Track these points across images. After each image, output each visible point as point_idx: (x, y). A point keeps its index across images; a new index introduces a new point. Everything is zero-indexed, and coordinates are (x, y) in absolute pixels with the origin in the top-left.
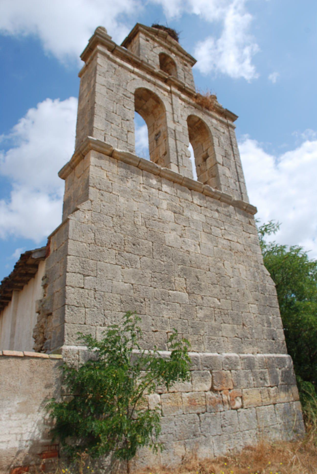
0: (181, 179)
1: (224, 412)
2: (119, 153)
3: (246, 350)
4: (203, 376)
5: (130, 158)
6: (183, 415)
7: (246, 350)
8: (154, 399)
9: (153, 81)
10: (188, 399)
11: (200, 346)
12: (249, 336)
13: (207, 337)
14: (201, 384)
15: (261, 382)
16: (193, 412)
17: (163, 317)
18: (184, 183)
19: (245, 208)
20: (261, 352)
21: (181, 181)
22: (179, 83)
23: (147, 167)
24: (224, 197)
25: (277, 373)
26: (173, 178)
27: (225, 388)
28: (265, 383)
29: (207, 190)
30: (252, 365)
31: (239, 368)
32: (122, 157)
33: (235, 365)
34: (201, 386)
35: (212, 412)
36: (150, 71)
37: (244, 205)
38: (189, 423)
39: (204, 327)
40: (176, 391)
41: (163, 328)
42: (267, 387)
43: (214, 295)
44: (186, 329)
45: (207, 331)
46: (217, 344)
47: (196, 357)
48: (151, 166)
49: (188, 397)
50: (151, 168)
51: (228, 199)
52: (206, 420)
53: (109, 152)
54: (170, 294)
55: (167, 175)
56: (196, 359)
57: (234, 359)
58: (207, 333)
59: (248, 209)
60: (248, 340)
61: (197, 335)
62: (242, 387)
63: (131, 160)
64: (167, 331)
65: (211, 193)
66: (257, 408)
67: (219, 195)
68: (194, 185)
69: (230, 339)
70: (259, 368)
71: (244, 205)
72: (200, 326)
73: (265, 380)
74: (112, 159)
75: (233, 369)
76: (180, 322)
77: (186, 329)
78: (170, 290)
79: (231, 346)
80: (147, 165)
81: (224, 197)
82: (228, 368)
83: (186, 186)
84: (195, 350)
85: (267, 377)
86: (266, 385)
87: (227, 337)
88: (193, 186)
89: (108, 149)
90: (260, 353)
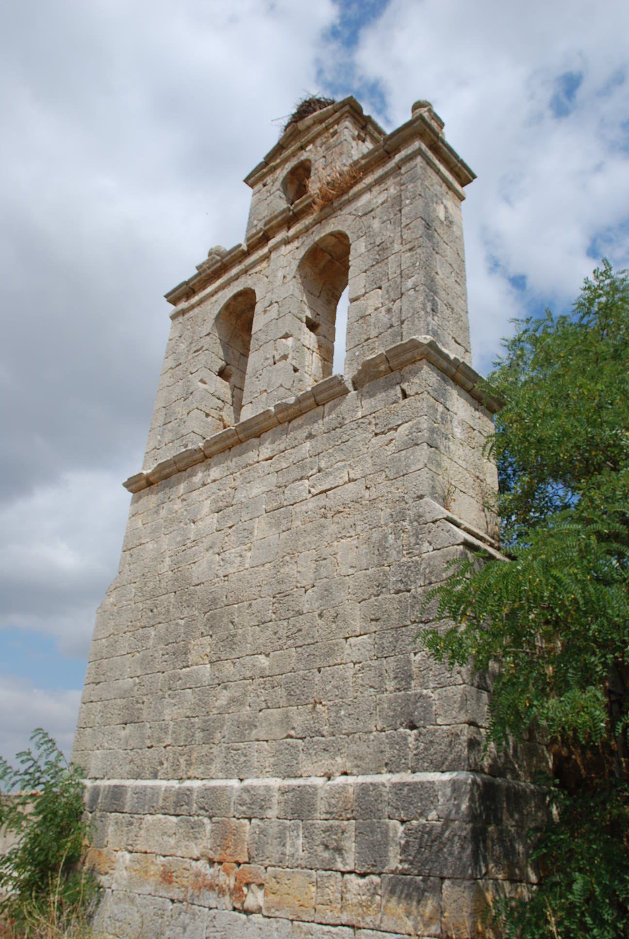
0: (233, 435)
1: (216, 911)
2: (153, 473)
3: (306, 766)
4: (193, 828)
5: (164, 469)
6: (149, 897)
7: (306, 766)
8: (121, 860)
9: (310, 224)
10: (162, 868)
11: (209, 766)
12: (326, 729)
13: (226, 745)
14: (187, 843)
15: (326, 855)
16: (165, 895)
17: (164, 720)
18: (241, 436)
19: (382, 368)
20: (355, 771)
21: (237, 437)
22: (280, 218)
23: (186, 461)
24: (321, 392)
25: (385, 834)
26: (223, 445)
27: (229, 858)
28: (339, 860)
29: (280, 412)
30: (306, 808)
31: (272, 813)
32: (157, 476)
33: (261, 808)
34: (186, 847)
35: (194, 904)
36: (240, 257)
37: (377, 366)
38: (154, 915)
39: (222, 727)
40: (149, 851)
41: (160, 740)
42: (343, 873)
43: (258, 647)
44: (193, 736)
45: (226, 733)
46: (243, 759)
47: (188, 790)
48: (188, 457)
49: (163, 865)
50: (190, 459)
51: (332, 387)
52: (182, 917)
53: (143, 482)
54: (181, 676)
55: (214, 448)
56: (188, 793)
57: (262, 792)
58: (227, 736)
59: (394, 363)
60: (323, 739)
61: (208, 744)
62: (267, 862)
63: (167, 471)
64: (165, 745)
65: (291, 411)
66: (295, 923)
67: (309, 398)
68: (257, 424)
69: (274, 743)
70: (324, 816)
71: (377, 366)
72: (217, 724)
73: (339, 850)
74: (152, 487)
75: (255, 817)
76: (185, 724)
77: (193, 736)
78: (184, 667)
79: (272, 760)
80: (184, 458)
81: (321, 392)
82: (244, 812)
83: (248, 438)
84: (198, 776)
85: (350, 845)
86: (340, 866)
87: (267, 741)
88: (256, 428)
89: (141, 480)
90: (351, 774)
